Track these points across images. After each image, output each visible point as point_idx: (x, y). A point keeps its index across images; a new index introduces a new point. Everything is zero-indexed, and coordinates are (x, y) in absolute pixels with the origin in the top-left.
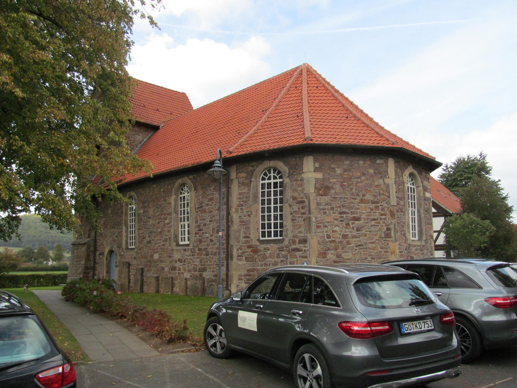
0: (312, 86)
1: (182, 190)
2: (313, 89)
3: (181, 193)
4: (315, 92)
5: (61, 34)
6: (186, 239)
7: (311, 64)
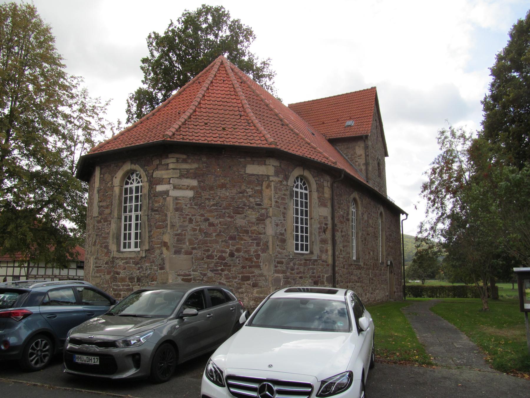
0: (219, 79)
1: (130, 179)
2: (220, 82)
3: (127, 183)
4: (221, 85)
5: (458, 231)
6: (133, 245)
7: (290, 103)
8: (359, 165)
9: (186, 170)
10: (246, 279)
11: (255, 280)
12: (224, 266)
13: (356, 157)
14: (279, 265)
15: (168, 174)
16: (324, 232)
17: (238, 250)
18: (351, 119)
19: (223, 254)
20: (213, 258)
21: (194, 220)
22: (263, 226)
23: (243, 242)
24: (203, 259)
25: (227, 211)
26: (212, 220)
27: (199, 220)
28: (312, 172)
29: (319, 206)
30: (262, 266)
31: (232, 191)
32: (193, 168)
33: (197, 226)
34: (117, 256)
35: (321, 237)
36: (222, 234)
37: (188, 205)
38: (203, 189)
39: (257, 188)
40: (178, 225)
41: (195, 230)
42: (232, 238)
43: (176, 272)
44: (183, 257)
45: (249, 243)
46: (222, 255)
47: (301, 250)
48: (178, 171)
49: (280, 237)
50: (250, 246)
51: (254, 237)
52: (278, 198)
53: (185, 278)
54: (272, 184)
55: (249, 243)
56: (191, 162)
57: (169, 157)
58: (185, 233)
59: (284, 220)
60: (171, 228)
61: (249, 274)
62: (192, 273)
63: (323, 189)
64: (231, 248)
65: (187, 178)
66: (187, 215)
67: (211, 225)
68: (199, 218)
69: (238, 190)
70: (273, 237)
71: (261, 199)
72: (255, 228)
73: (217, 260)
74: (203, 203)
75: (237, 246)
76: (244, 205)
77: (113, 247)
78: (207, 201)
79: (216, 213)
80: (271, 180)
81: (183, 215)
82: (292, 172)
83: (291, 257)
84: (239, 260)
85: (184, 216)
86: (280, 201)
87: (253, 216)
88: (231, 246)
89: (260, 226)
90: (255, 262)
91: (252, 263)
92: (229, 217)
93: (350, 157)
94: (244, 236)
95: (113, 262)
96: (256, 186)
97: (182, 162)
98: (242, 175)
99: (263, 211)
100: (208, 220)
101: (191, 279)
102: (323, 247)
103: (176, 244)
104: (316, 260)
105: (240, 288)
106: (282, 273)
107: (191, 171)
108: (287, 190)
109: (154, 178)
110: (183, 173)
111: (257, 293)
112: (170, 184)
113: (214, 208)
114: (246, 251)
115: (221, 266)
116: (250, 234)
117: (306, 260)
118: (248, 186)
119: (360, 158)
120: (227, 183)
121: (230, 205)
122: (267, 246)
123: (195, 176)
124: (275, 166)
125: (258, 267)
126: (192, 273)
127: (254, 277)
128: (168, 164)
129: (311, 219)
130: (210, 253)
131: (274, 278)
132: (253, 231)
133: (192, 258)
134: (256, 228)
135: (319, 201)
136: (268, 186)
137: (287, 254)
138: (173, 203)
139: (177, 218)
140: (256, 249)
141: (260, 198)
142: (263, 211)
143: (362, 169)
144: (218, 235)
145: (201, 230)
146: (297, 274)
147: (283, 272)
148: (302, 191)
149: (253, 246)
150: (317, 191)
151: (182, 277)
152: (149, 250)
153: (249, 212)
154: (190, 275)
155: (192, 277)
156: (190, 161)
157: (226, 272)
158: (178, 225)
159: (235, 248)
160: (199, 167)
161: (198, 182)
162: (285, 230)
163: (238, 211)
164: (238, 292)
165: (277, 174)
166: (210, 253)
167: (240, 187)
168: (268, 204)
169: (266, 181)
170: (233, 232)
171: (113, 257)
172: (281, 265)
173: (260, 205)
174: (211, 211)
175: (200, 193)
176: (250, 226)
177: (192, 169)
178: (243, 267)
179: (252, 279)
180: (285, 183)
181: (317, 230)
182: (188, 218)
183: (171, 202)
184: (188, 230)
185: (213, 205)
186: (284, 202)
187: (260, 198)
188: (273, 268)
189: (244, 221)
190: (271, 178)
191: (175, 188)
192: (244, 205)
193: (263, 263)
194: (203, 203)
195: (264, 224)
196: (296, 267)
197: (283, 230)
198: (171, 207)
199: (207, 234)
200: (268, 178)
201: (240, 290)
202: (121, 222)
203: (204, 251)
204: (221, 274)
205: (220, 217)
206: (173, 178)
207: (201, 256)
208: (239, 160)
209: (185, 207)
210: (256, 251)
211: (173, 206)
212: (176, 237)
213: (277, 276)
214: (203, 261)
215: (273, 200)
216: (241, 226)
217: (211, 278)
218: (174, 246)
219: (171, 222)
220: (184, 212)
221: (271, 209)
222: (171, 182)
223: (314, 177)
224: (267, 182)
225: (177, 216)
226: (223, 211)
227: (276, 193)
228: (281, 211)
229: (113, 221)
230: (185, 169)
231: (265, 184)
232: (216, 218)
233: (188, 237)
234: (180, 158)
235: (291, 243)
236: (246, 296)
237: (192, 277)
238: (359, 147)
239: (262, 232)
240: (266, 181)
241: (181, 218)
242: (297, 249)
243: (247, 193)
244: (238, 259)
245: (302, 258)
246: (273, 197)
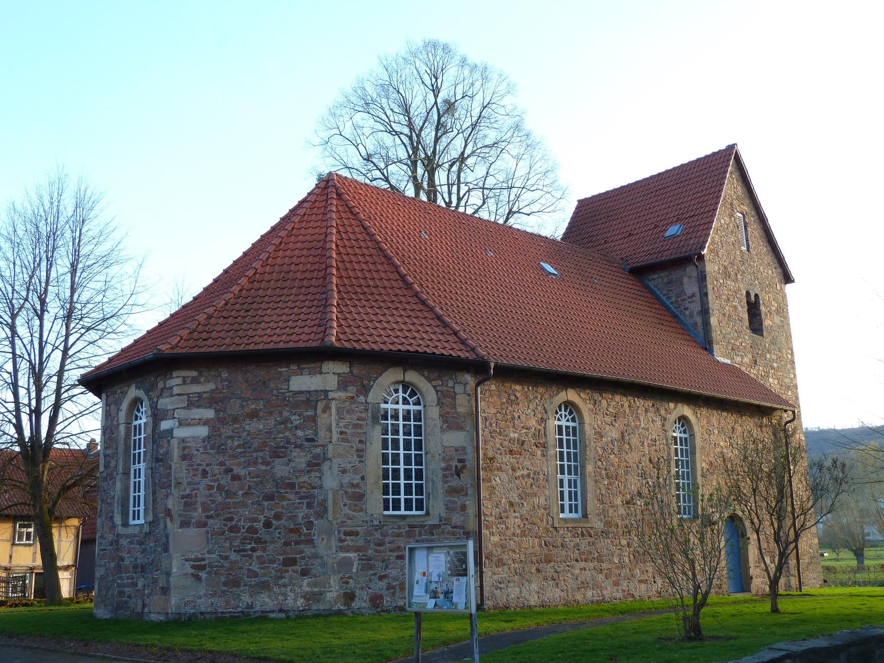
7: (582, 197)
8: (691, 316)
9: (197, 395)
10: (290, 562)
11: (306, 565)
12: (255, 543)
13: (685, 300)
14: (348, 538)
15: (172, 403)
16: (458, 473)
17: (278, 517)
18: (678, 220)
19: (254, 524)
20: (239, 531)
21: (210, 472)
22: (318, 474)
23: (285, 503)
24: (224, 533)
25: (261, 454)
26: (237, 470)
27: (217, 471)
28: (426, 373)
29: (443, 431)
30: (316, 541)
31: (268, 421)
32: (208, 390)
33: (214, 481)
34: (122, 533)
35: (449, 484)
36: (253, 491)
37: (201, 450)
38: (223, 421)
39: (308, 413)
40: (185, 482)
41: (210, 488)
42: (269, 497)
43: (184, 555)
44: (193, 531)
45: (294, 503)
46: (253, 526)
47: (406, 510)
48: (186, 397)
49: (350, 490)
50: (297, 508)
51: (302, 494)
52: (346, 426)
53: (196, 563)
54: (333, 405)
55: (294, 503)
56: (205, 380)
57: (174, 376)
58: (196, 493)
59: (361, 462)
60: (175, 487)
61: (296, 554)
62: (207, 556)
63: (454, 399)
64: (267, 513)
65: (198, 407)
66: (199, 465)
67: (236, 478)
68: (216, 469)
69: (278, 419)
70: (336, 492)
71: (315, 430)
72: (304, 478)
73: (246, 534)
74: (222, 444)
75: (276, 510)
76: (288, 443)
77: (118, 519)
78: (229, 442)
79: (243, 460)
80: (330, 397)
81: (193, 465)
82: (377, 378)
83: (376, 523)
84: (279, 533)
85: (195, 467)
86: (349, 431)
87: (301, 459)
88: (266, 510)
89: (313, 474)
90: (305, 535)
91: (300, 536)
92: (263, 463)
93: (674, 299)
94: (287, 493)
95: (117, 542)
96: (307, 410)
97: (191, 383)
98: (283, 393)
99: (318, 450)
100: (231, 470)
101: (205, 565)
102: (454, 502)
103: (184, 511)
104: (437, 526)
105: (282, 577)
106: (355, 551)
107: (205, 395)
108: (367, 410)
109: (159, 410)
110: (192, 399)
111: (308, 585)
112: (174, 418)
113: (240, 450)
114: (290, 518)
115: (251, 544)
116: (297, 490)
117: (410, 526)
118: (294, 411)
119: (692, 302)
120: (260, 410)
121: (264, 444)
122: (325, 508)
123: (211, 401)
124: (339, 375)
125: (310, 542)
126: (207, 556)
127: (304, 559)
128: (171, 388)
129: (426, 454)
130: (234, 523)
131: (337, 560)
132: (301, 484)
133: (208, 532)
134: (307, 479)
135: (445, 422)
136: (327, 408)
137: (368, 518)
138: (178, 448)
139: (185, 471)
140: (306, 512)
141: (314, 428)
142: (318, 450)
143: (696, 323)
144: (246, 494)
145: (220, 488)
146: (391, 551)
147: (357, 549)
148: (407, 407)
149: (302, 508)
150: (438, 404)
151: (192, 563)
152: (153, 522)
153: (294, 454)
154: (204, 559)
155: (207, 562)
156: (202, 380)
157: (259, 553)
158: (185, 482)
159: (273, 513)
160: (217, 389)
161: (215, 411)
162: (363, 478)
163: (276, 454)
164: (278, 584)
165: (343, 385)
166: (234, 523)
167: (281, 414)
168: (325, 438)
169: (323, 399)
170: (269, 488)
171: (118, 534)
172: (353, 537)
173: (312, 440)
174: (235, 457)
175: (219, 429)
176: (296, 476)
177: (205, 392)
178: (286, 544)
179: (300, 562)
180: (362, 399)
181: (440, 474)
182: (200, 470)
183: (176, 446)
184: (201, 489)
185: (239, 446)
186: (360, 431)
187: (314, 428)
188: (334, 543)
189: (287, 468)
190: (331, 395)
191: (181, 424)
192: (288, 443)
193: (319, 535)
194: (222, 444)
195: (320, 471)
196: (387, 539)
197: (359, 477)
198: (176, 453)
199: (229, 494)
200: (326, 395)
201: (281, 582)
202: (128, 478)
203: (224, 520)
204: (250, 557)
205: (249, 465)
206: (178, 408)
207: (220, 528)
208: (279, 370)
209: (195, 452)
210: (307, 516)
211: (179, 452)
212: (183, 501)
213: (345, 557)
214: (223, 537)
215: (334, 429)
216: (282, 477)
217: (236, 562)
218: (179, 515)
219: (175, 478)
220: (194, 460)
221: (330, 447)
222: (176, 415)
223: (430, 382)
224: (324, 402)
225: (184, 467)
226: (255, 455)
227: (342, 419)
228: (352, 447)
229: (118, 478)
230: (196, 393)
231: (320, 406)
232: (243, 468)
233: (200, 499)
234: (187, 377)
235: (374, 501)
236: (291, 590)
237: (207, 562)
238: (690, 277)
239: (316, 485)
240: (323, 399)
241: (191, 471)
242: (386, 508)
243: (292, 423)
244: (278, 531)
245: (403, 523)
246: (334, 425)
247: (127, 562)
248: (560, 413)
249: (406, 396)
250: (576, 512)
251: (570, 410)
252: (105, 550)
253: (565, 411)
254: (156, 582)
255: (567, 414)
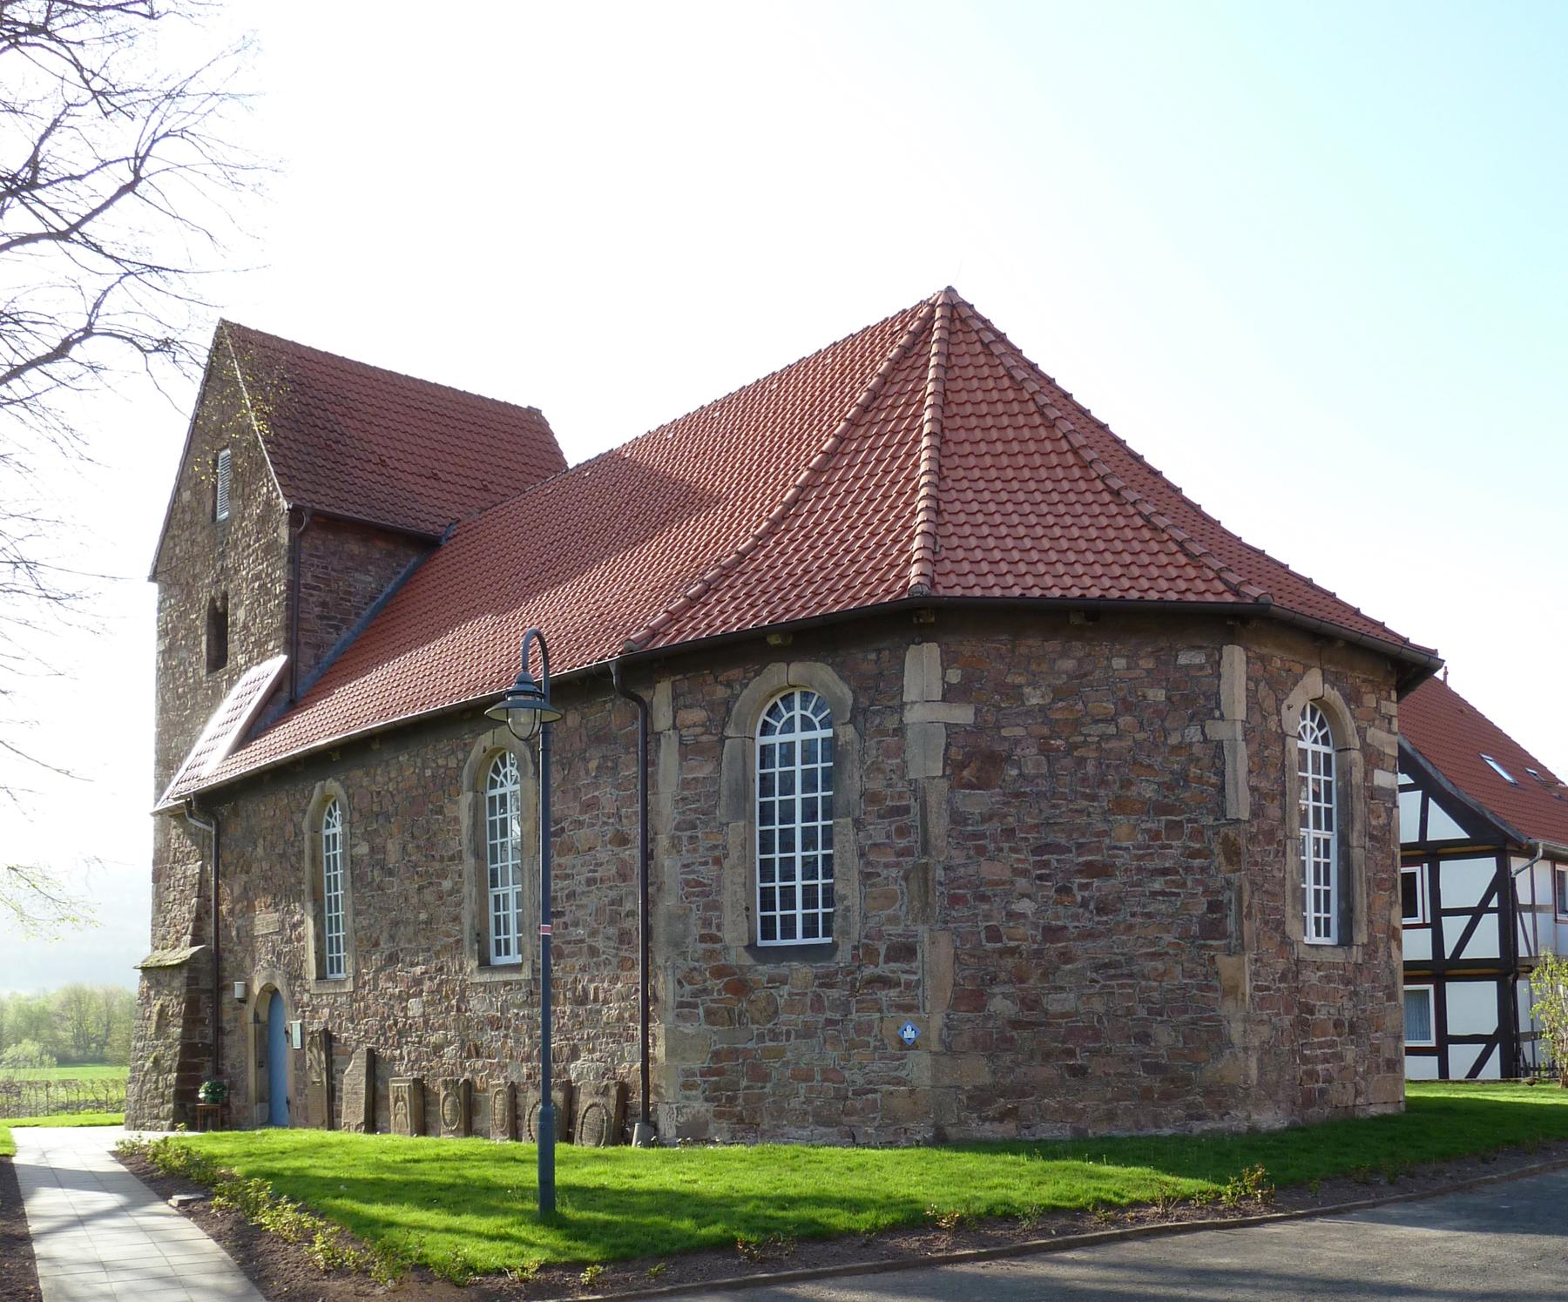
3: (493, 784)
34: (1309, 959)
247: (1321, 1015)
248: (1302, 723)
249: (808, 713)
250: (1327, 934)
251: (1321, 718)
252: (1268, 988)
253: (1312, 720)
254: (1378, 1050)
255: (1315, 726)
